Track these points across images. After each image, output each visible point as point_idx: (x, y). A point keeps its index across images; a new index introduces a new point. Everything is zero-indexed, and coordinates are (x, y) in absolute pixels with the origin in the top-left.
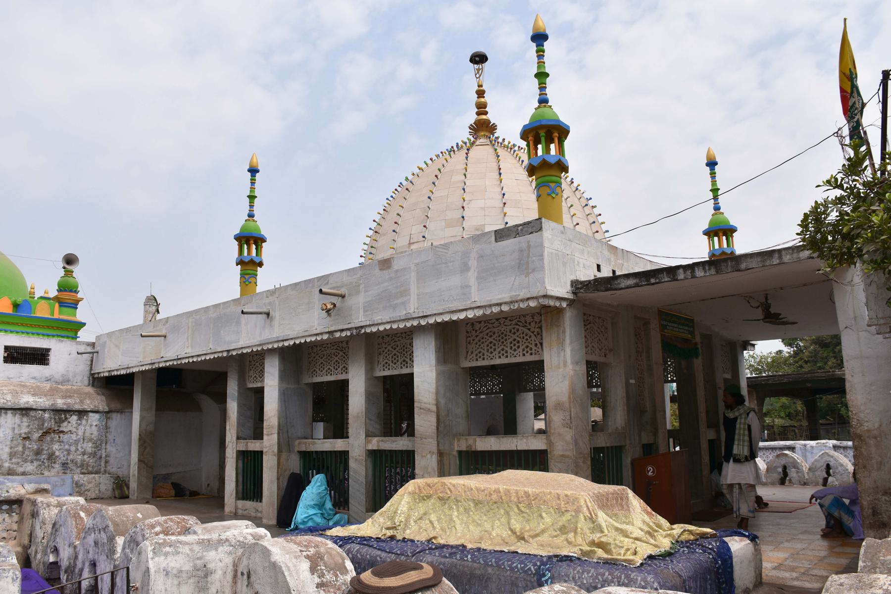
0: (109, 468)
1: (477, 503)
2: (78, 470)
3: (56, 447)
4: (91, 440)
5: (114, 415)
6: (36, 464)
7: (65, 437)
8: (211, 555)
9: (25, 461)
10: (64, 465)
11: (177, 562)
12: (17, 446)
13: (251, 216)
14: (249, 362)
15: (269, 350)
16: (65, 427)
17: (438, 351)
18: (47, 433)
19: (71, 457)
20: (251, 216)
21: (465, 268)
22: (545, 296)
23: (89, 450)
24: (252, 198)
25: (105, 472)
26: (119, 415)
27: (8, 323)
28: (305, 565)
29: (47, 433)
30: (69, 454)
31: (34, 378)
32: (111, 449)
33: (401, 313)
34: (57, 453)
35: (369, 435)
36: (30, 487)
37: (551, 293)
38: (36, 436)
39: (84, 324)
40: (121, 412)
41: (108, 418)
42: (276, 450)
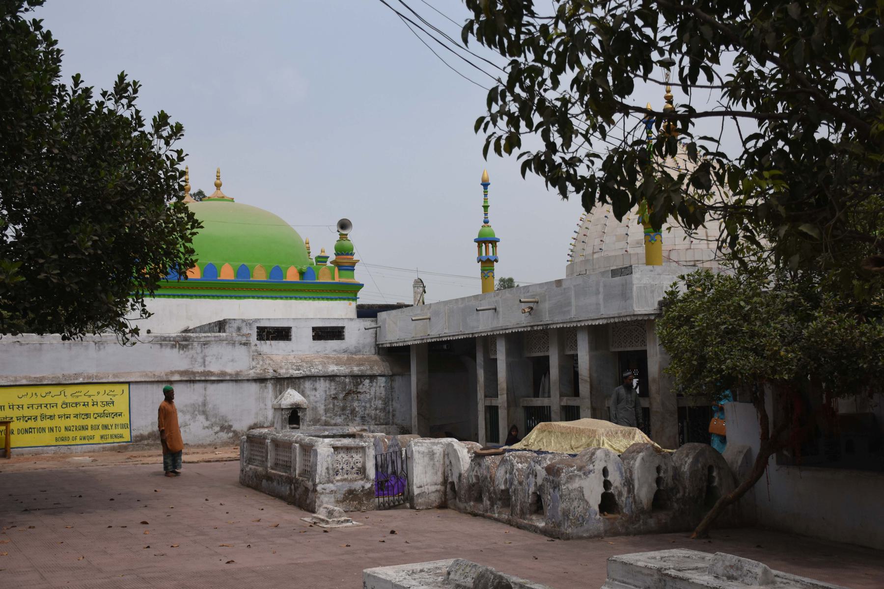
0: (395, 420)
1: (562, 433)
2: (373, 422)
3: (356, 404)
4: (380, 398)
5: (397, 378)
6: (343, 417)
7: (361, 397)
8: (435, 447)
9: (336, 415)
10: (363, 418)
11: (422, 449)
12: (329, 404)
13: (486, 222)
14: (488, 341)
15: (500, 334)
16: (361, 389)
17: (590, 343)
18: (348, 394)
19: (367, 412)
20: (486, 222)
21: (597, 293)
22: (634, 315)
23: (380, 406)
24: (486, 207)
25: (393, 424)
26: (400, 378)
27: (297, 290)
28: (466, 450)
29: (348, 394)
30: (365, 410)
31: (335, 351)
32: (396, 405)
33: (567, 318)
34: (357, 409)
35: (562, 395)
36: (358, 428)
37: (636, 313)
38: (341, 396)
39: (362, 285)
40: (401, 375)
41: (392, 381)
42: (506, 405)
